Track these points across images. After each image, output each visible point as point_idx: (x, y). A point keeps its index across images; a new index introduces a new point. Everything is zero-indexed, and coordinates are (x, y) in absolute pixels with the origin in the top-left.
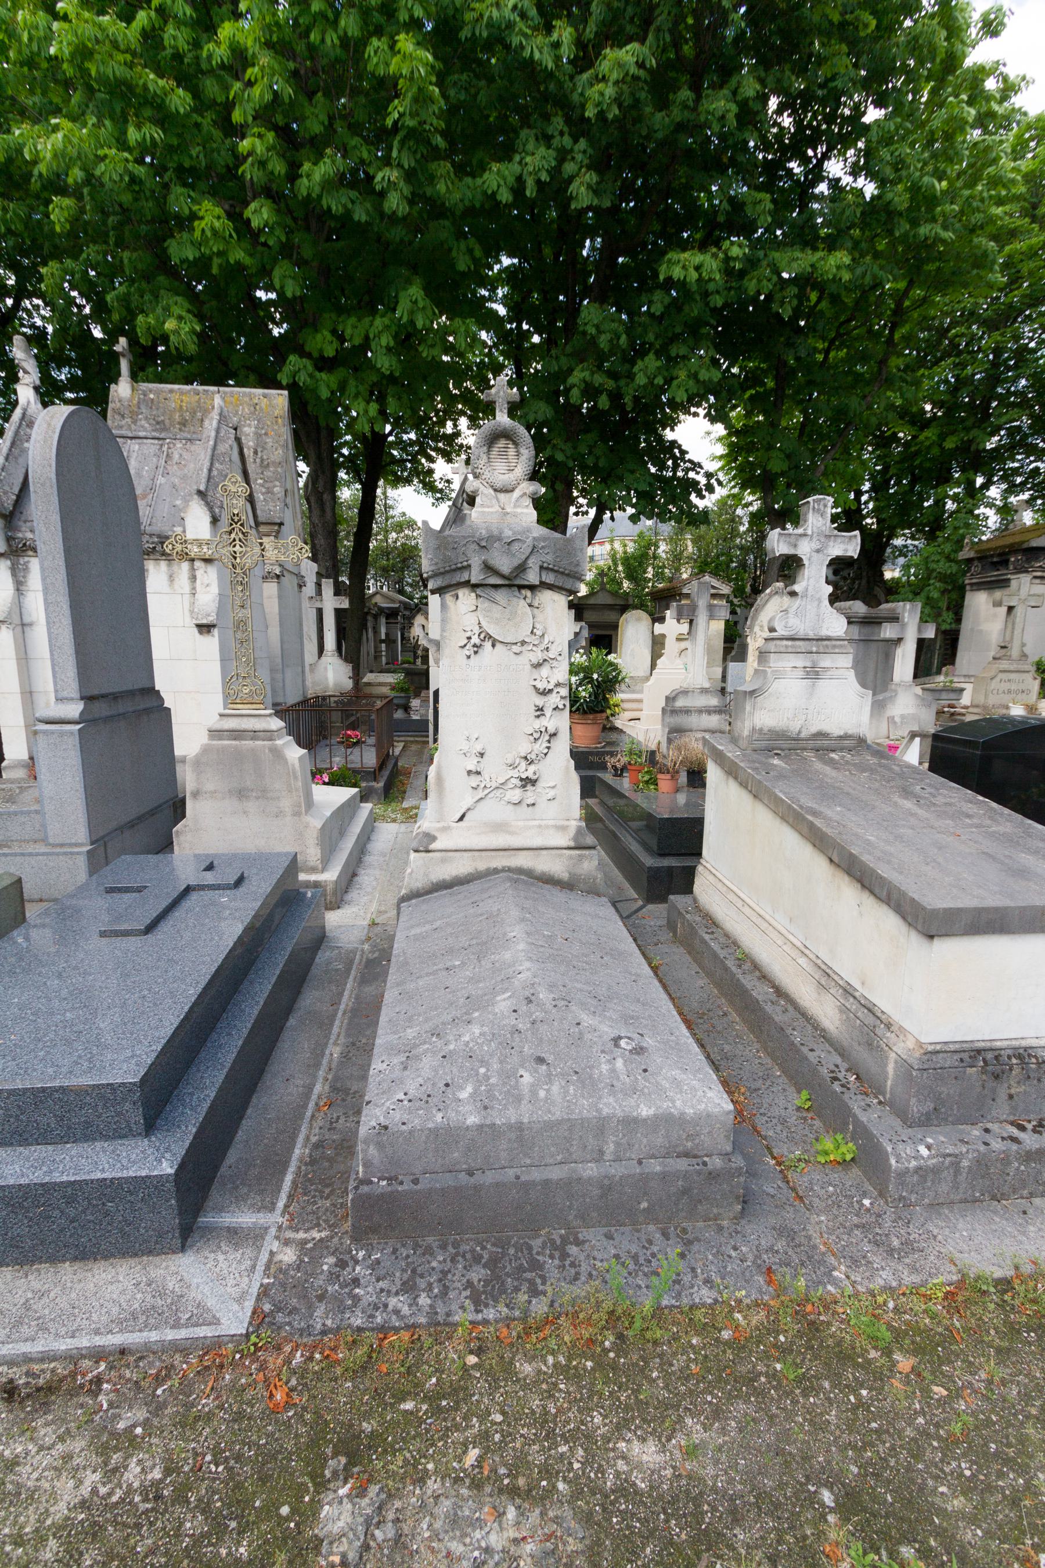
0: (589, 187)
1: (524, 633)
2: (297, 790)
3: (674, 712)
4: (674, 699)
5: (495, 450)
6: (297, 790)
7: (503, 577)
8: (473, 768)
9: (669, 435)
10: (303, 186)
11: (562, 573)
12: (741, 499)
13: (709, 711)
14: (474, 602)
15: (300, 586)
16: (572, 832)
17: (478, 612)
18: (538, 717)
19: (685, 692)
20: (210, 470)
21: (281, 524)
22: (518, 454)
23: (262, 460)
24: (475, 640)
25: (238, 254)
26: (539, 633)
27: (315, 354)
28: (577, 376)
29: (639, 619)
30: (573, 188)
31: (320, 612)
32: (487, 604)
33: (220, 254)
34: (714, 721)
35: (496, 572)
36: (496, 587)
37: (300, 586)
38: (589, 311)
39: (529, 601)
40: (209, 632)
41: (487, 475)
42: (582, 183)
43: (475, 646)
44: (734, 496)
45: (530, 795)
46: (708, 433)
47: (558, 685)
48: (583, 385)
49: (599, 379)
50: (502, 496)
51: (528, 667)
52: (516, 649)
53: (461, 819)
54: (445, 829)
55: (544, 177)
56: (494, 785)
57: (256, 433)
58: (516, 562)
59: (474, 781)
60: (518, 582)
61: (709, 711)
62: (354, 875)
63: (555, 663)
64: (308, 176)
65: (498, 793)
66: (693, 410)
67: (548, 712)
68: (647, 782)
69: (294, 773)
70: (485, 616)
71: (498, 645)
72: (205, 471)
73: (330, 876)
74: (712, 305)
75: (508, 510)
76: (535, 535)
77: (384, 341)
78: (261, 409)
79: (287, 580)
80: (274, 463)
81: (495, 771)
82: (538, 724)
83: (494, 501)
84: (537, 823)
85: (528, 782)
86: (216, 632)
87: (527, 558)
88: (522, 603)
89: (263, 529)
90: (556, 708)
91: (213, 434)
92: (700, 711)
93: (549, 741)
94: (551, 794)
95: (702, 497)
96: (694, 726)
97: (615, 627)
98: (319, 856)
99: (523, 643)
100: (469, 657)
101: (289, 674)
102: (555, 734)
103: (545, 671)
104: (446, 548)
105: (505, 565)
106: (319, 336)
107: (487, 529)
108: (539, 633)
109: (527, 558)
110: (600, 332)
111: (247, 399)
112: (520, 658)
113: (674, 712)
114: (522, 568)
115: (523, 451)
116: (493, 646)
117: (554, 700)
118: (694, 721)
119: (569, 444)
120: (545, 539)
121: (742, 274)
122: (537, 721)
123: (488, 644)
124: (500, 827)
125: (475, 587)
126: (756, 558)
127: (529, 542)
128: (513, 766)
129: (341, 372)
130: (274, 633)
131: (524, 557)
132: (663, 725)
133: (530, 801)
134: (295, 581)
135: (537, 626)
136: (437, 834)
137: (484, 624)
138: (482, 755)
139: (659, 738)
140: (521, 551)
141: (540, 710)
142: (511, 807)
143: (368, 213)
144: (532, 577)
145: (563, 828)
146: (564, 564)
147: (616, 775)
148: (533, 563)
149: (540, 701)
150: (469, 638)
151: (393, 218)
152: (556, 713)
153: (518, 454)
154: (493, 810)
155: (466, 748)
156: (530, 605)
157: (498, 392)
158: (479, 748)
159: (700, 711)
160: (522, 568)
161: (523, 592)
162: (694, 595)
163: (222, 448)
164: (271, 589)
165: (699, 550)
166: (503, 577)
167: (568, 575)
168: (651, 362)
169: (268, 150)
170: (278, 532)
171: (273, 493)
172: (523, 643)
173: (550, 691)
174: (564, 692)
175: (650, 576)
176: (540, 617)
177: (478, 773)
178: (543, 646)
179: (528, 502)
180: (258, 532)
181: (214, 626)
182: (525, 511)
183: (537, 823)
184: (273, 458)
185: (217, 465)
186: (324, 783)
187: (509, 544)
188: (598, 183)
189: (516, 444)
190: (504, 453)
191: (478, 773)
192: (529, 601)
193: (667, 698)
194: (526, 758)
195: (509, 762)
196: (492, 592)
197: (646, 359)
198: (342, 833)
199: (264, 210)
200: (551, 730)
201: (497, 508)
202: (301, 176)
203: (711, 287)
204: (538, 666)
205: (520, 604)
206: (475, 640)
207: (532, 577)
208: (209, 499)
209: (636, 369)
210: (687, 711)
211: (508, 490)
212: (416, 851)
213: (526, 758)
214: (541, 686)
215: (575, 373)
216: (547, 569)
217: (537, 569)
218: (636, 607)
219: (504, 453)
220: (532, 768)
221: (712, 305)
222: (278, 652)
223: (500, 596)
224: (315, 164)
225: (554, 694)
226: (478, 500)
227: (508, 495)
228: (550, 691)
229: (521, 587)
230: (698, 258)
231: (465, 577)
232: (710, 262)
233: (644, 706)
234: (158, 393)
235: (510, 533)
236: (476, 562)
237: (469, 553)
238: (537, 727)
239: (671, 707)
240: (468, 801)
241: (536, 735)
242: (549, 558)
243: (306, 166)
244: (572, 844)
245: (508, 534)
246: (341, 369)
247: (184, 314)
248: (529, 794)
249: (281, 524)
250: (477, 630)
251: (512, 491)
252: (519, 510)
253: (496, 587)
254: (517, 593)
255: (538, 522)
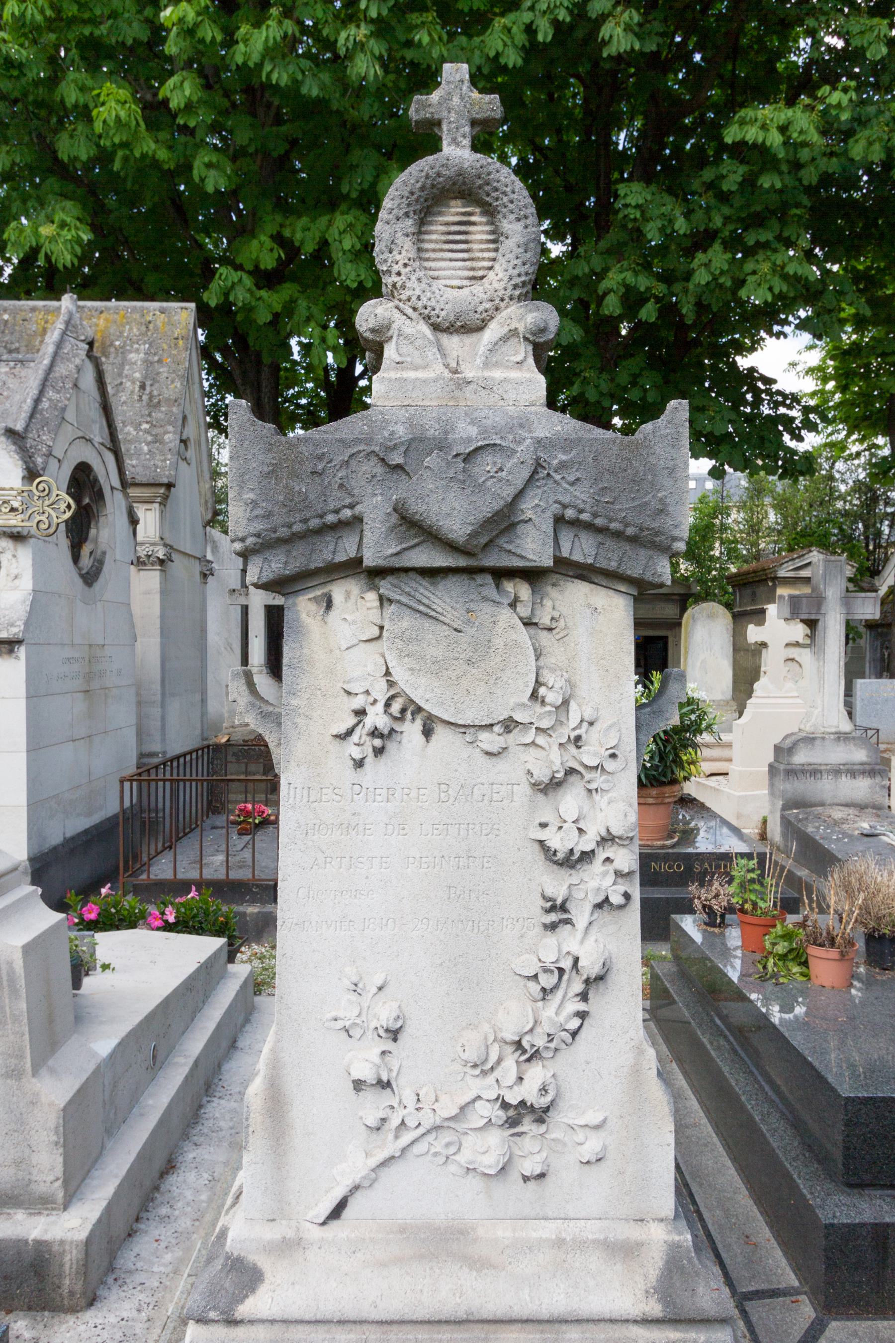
0: (628, 28)
1: (511, 699)
2: (16, 1019)
3: (792, 773)
4: (791, 750)
5: (437, 230)
6: (16, 1019)
7: (452, 547)
8: (365, 1072)
9: (743, 362)
10: (239, 53)
11: (618, 535)
12: (844, 448)
13: (853, 771)
14: (374, 615)
15: (205, 576)
16: (653, 1264)
17: (384, 644)
18: (552, 927)
19: (809, 740)
20: (37, 401)
21: (169, 486)
22: (497, 237)
23: (151, 397)
24: (377, 718)
25: (148, 145)
26: (553, 697)
27: (249, 267)
28: (614, 279)
29: (711, 616)
30: (605, 32)
31: (245, 610)
32: (407, 621)
33: (125, 145)
34: (860, 788)
35: (431, 536)
36: (431, 573)
37: (205, 576)
38: (633, 195)
39: (524, 610)
40: (11, 651)
41: (414, 288)
42: (617, 24)
43: (375, 733)
44: (831, 445)
45: (531, 1151)
46: (793, 365)
47: (608, 839)
48: (623, 290)
49: (643, 282)
50: (453, 343)
51: (524, 790)
52: (490, 740)
53: (337, 1212)
54: (289, 1247)
55: (562, 15)
56: (428, 1120)
57: (145, 361)
58: (487, 507)
59: (372, 1107)
60: (493, 560)
61: (853, 771)
62: (170, 1167)
63: (598, 780)
64: (246, 41)
65: (438, 1143)
66: (776, 328)
67: (581, 914)
68: (783, 957)
69: (12, 981)
70: (402, 655)
71: (440, 732)
72: (29, 402)
73: (70, 1227)
74: (805, 183)
75: (469, 374)
76: (541, 432)
77: (347, 245)
78: (156, 329)
79: (179, 565)
80: (168, 400)
81: (434, 1076)
82: (550, 949)
83: (432, 353)
84: (547, 1230)
85: (518, 1115)
86: (22, 651)
87: (519, 495)
88: (506, 616)
89: (133, 492)
90: (603, 904)
91: (51, 349)
92: (837, 772)
93: (584, 997)
94: (592, 1146)
95: (800, 439)
96: (828, 797)
97: (676, 625)
98: (59, 1171)
99: (509, 725)
100: (359, 764)
101: (175, 708)
102: (600, 978)
103: (570, 802)
104: (294, 475)
105: (455, 512)
106: (255, 243)
107: (410, 423)
108: (553, 697)
109: (519, 495)
110: (646, 219)
111: (136, 316)
112: (501, 765)
113: (792, 773)
114: (504, 522)
115: (509, 225)
116: (427, 732)
117: (596, 880)
118: (826, 788)
119: (604, 376)
120: (567, 444)
121: (848, 134)
122: (551, 940)
123: (412, 729)
124: (443, 1242)
125: (376, 574)
126: (866, 527)
127: (525, 451)
128: (483, 1067)
129: (288, 290)
130: (149, 647)
131: (508, 493)
132: (772, 794)
133: (530, 1167)
134: (197, 568)
135: (549, 678)
136: (263, 1262)
137: (398, 675)
138: (394, 1034)
139: (765, 812)
140: (500, 478)
141: (558, 912)
142: (475, 1183)
143: (323, 87)
144: (534, 546)
145: (626, 1251)
146: (623, 511)
147: (711, 924)
148: (537, 510)
149: (557, 885)
150: (361, 713)
151: (360, 91)
152: (605, 916)
153: (497, 237)
154: (425, 1191)
155: (349, 1014)
156: (528, 623)
157: (448, 97)
158: (385, 1015)
159: (837, 772)
160: (504, 522)
161: (509, 586)
162: (818, 579)
163: (63, 369)
164: (147, 583)
165: (785, 518)
166: (452, 547)
167: (634, 540)
168: (719, 256)
169: (198, 14)
170: (166, 498)
171: (162, 442)
172: (509, 725)
173: (587, 856)
174: (626, 859)
175: (717, 554)
176: (556, 654)
177: (384, 1085)
178: (564, 733)
179: (522, 352)
180: (126, 496)
181: (20, 642)
182: (514, 374)
183: (547, 1230)
184: (166, 394)
185: (50, 393)
186: (168, 927)
187: (468, 458)
188: (640, 25)
189: (490, 212)
190: (458, 238)
191: (384, 1085)
192: (524, 610)
193: (778, 749)
194: (518, 1045)
195: (472, 1055)
196: (423, 589)
197: (710, 252)
198: (113, 1125)
199: (187, 85)
200: (590, 965)
201: (438, 369)
202: (237, 42)
203: (804, 155)
204: (550, 787)
205: (501, 621)
206: (377, 718)
207: (534, 546)
208: (29, 443)
209: (695, 264)
210: (814, 772)
211: (467, 326)
212: (201, 1320)
213: (518, 1045)
214: (559, 842)
215: (610, 274)
216: (575, 523)
217: (547, 526)
218: (699, 599)
219: (458, 238)
220: (536, 1074)
221: (805, 183)
222: (156, 675)
223: (445, 599)
224: (257, 25)
225: (597, 865)
226: (390, 352)
227: (469, 340)
228: (587, 856)
229: (501, 574)
230: (786, 114)
231: (347, 549)
232: (802, 120)
233: (736, 753)
234: (14, 312)
235: (473, 431)
236: (375, 509)
237: (358, 484)
238: (549, 957)
239: (784, 763)
240: (353, 1166)
241: (547, 981)
242: (581, 495)
243: (244, 29)
244: (655, 1309)
245: (467, 432)
246: (287, 285)
247: (68, 220)
248: (528, 1144)
249: (169, 486)
250: (381, 692)
251: (480, 329)
252: (498, 374)
253: (431, 573)
254: (491, 591)
255: (551, 403)
